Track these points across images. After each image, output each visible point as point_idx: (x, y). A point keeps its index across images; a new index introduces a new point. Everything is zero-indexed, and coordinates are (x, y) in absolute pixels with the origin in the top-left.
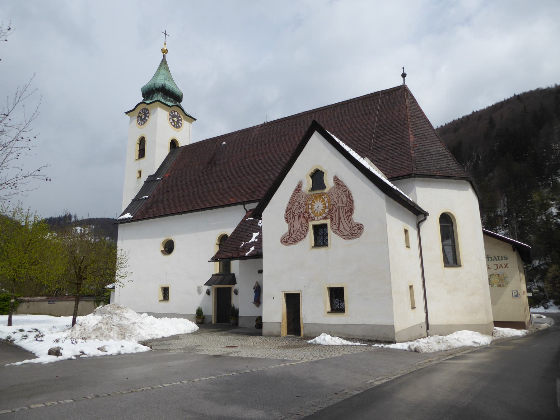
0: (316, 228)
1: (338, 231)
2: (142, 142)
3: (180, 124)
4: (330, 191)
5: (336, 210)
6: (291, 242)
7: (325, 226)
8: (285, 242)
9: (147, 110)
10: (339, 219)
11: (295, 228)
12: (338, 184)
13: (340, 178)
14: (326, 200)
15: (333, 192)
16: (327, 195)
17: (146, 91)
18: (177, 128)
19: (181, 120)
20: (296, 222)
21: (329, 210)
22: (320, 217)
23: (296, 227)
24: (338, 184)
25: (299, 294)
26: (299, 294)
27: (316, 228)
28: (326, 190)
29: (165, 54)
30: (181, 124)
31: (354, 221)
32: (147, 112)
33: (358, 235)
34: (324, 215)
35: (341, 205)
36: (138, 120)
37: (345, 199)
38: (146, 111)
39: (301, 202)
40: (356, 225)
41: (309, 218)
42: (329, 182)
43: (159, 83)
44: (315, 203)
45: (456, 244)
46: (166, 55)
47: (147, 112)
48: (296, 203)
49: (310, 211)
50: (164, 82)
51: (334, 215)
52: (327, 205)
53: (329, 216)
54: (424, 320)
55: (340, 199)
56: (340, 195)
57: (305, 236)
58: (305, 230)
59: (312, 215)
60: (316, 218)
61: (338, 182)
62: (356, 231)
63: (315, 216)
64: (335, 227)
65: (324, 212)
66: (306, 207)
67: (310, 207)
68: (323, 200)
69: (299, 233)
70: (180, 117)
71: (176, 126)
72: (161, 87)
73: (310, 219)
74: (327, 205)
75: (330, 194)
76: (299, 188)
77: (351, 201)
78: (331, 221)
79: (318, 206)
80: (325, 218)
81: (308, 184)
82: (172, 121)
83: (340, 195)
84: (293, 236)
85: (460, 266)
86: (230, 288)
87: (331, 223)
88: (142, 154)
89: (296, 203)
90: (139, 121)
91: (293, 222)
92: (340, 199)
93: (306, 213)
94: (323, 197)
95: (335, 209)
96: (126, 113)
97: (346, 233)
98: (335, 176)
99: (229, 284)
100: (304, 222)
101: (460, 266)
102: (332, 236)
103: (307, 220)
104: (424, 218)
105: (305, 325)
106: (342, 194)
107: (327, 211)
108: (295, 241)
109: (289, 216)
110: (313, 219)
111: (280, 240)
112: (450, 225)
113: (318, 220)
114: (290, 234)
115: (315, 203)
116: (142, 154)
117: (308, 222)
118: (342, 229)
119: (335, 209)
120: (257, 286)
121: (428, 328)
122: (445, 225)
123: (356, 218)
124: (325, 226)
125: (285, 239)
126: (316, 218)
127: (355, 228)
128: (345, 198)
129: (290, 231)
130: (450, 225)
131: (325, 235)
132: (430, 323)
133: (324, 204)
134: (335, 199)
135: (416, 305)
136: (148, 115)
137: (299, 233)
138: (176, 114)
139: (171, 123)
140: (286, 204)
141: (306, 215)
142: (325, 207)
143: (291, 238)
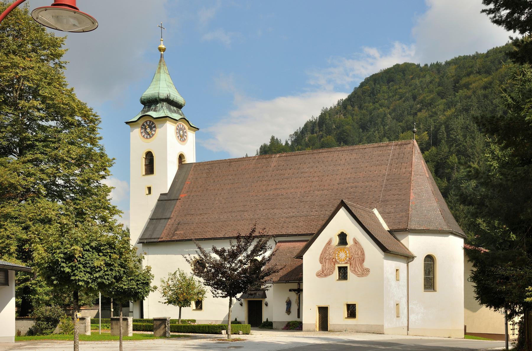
0: (340, 268)
1: (354, 272)
2: (150, 157)
3: (185, 137)
4: (350, 247)
5: (354, 259)
6: (323, 276)
7: (347, 267)
9: (153, 123)
10: (355, 265)
11: (326, 268)
12: (356, 243)
13: (357, 240)
14: (347, 252)
16: (348, 248)
17: (147, 99)
18: (183, 141)
19: (186, 132)
20: (327, 264)
21: (349, 259)
22: (344, 262)
23: (327, 267)
24: (356, 243)
25: (327, 308)
26: (327, 308)
27: (340, 268)
28: (347, 246)
29: (162, 53)
30: (186, 136)
31: (365, 267)
32: (153, 126)
33: (367, 275)
34: (346, 261)
35: (357, 256)
36: (142, 133)
39: (331, 251)
41: (336, 262)
42: (349, 240)
43: (163, 94)
44: (340, 253)
45: (435, 276)
47: (153, 126)
49: (337, 258)
50: (168, 92)
51: (352, 262)
52: (348, 255)
53: (349, 262)
54: (406, 325)
56: (357, 250)
57: (333, 273)
58: (333, 269)
59: (338, 261)
60: (341, 262)
61: (356, 242)
62: (365, 273)
63: (340, 261)
64: (352, 269)
65: (346, 260)
66: (334, 255)
67: (337, 255)
68: (346, 252)
69: (329, 271)
70: (185, 129)
72: (166, 98)
74: (348, 255)
75: (351, 248)
76: (329, 243)
77: (363, 254)
78: (350, 265)
79: (342, 255)
80: (347, 263)
81: (336, 240)
82: (178, 135)
83: (357, 250)
84: (325, 272)
85: (436, 291)
86: (261, 301)
87: (350, 267)
88: (150, 169)
90: (144, 134)
91: (325, 264)
93: (334, 258)
94: (346, 250)
95: (353, 258)
96: (127, 123)
97: (359, 273)
99: (262, 298)
100: (333, 264)
101: (436, 291)
103: (335, 263)
106: (358, 250)
107: (347, 259)
108: (326, 276)
109: (322, 259)
110: (339, 263)
111: (315, 274)
112: (432, 263)
113: (342, 264)
114: (323, 271)
115: (340, 253)
116: (150, 169)
117: (335, 265)
118: (357, 270)
119: (353, 258)
121: (408, 330)
122: (428, 263)
123: (366, 265)
124: (347, 267)
125: (319, 273)
127: (365, 271)
128: (360, 252)
129: (323, 269)
130: (432, 263)
133: (346, 254)
134: (353, 252)
137: (329, 271)
138: (182, 127)
140: (320, 252)
141: (334, 260)
142: (347, 257)
143: (323, 274)
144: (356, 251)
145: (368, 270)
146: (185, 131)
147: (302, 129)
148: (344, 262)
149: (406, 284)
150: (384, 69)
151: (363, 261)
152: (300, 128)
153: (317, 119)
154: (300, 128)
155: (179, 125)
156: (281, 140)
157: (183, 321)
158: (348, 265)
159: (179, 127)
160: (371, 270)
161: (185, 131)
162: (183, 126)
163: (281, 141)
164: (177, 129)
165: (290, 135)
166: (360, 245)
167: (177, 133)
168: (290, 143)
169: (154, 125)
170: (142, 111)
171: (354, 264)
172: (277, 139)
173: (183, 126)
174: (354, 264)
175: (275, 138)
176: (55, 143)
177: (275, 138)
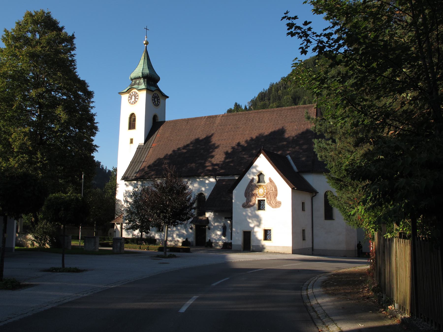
1: (270, 204)
5: (269, 194)
7: (264, 200)
8: (244, 207)
12: (271, 182)
14: (265, 188)
15: (268, 185)
16: (266, 186)
19: (159, 99)
21: (266, 194)
22: (262, 196)
24: (271, 182)
25: (250, 232)
32: (136, 95)
33: (279, 206)
34: (264, 196)
37: (274, 189)
38: (136, 94)
40: (278, 202)
46: (147, 46)
47: (136, 95)
48: (250, 188)
53: (266, 196)
54: (311, 246)
55: (271, 189)
60: (260, 196)
61: (271, 181)
62: (278, 205)
64: (268, 202)
68: (264, 188)
70: (158, 97)
71: (156, 105)
73: (257, 197)
77: (276, 190)
78: (267, 198)
80: (264, 197)
82: (153, 101)
89: (250, 188)
91: (248, 198)
92: (271, 189)
97: (273, 205)
98: (270, 178)
102: (267, 206)
104: (315, 195)
105: (253, 246)
107: (265, 194)
113: (261, 197)
117: (256, 198)
118: (272, 203)
120: (224, 226)
123: (278, 198)
124: (264, 200)
125: (244, 205)
126: (260, 196)
127: (278, 203)
128: (274, 189)
131: (264, 205)
132: (314, 248)
134: (269, 189)
135: (306, 238)
136: (137, 97)
138: (156, 96)
139: (153, 103)
144: (271, 188)
145: (280, 203)
146: (159, 98)
147: (257, 98)
148: (262, 196)
149: (310, 213)
150: (312, 56)
151: (276, 195)
152: (255, 97)
153: (267, 91)
154: (255, 97)
155: (154, 94)
156: (242, 106)
157: (81, 246)
158: (265, 199)
159: (154, 96)
160: (282, 203)
161: (159, 98)
162: (157, 95)
163: (241, 106)
164: (153, 97)
165: (248, 102)
166: (274, 183)
167: (153, 100)
168: (248, 107)
169: (137, 95)
170: (130, 85)
171: (269, 198)
172: (239, 105)
173: (157, 95)
174: (269, 198)
175: (238, 104)
176: (335, 119)
177: (238, 104)
